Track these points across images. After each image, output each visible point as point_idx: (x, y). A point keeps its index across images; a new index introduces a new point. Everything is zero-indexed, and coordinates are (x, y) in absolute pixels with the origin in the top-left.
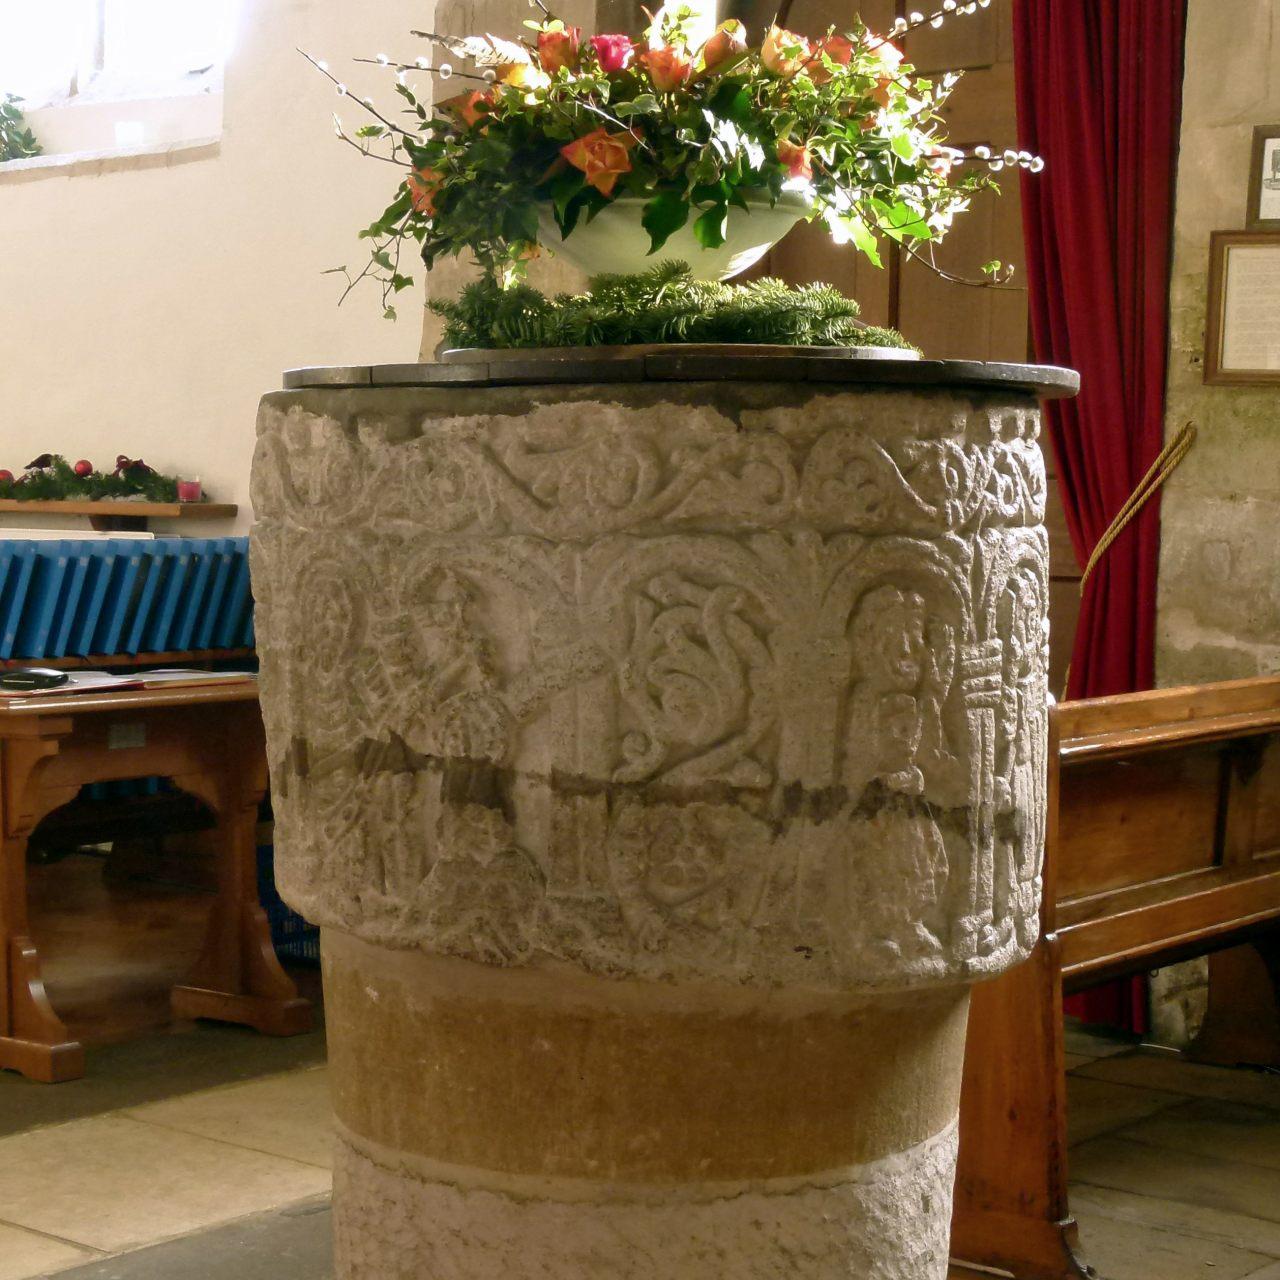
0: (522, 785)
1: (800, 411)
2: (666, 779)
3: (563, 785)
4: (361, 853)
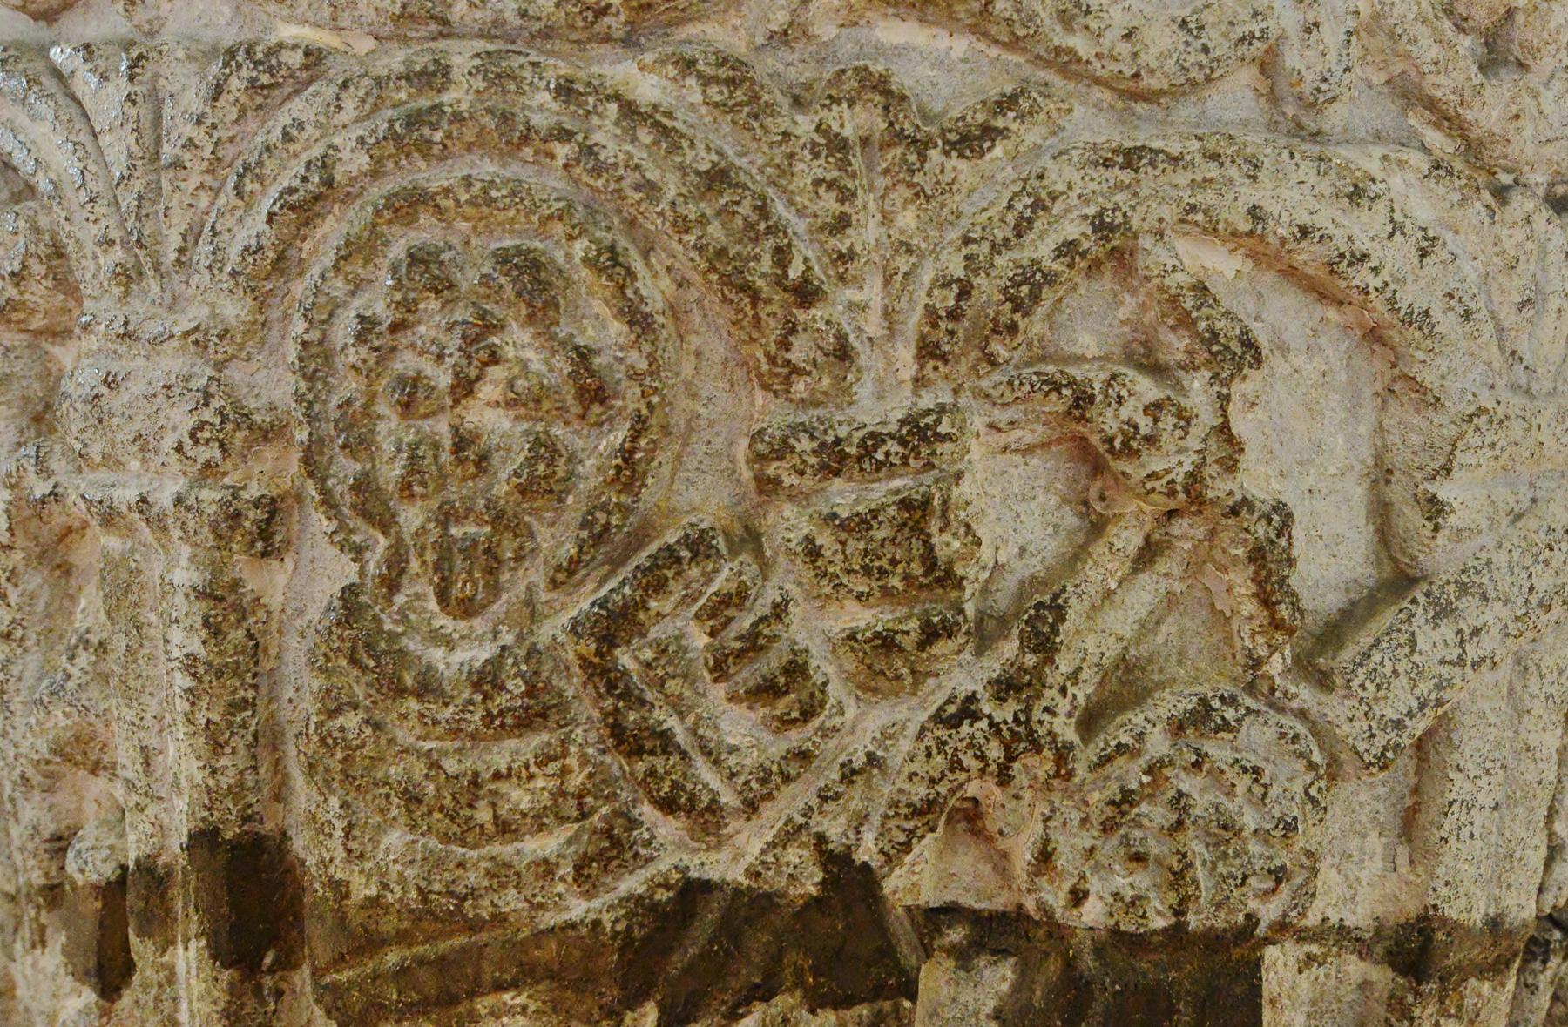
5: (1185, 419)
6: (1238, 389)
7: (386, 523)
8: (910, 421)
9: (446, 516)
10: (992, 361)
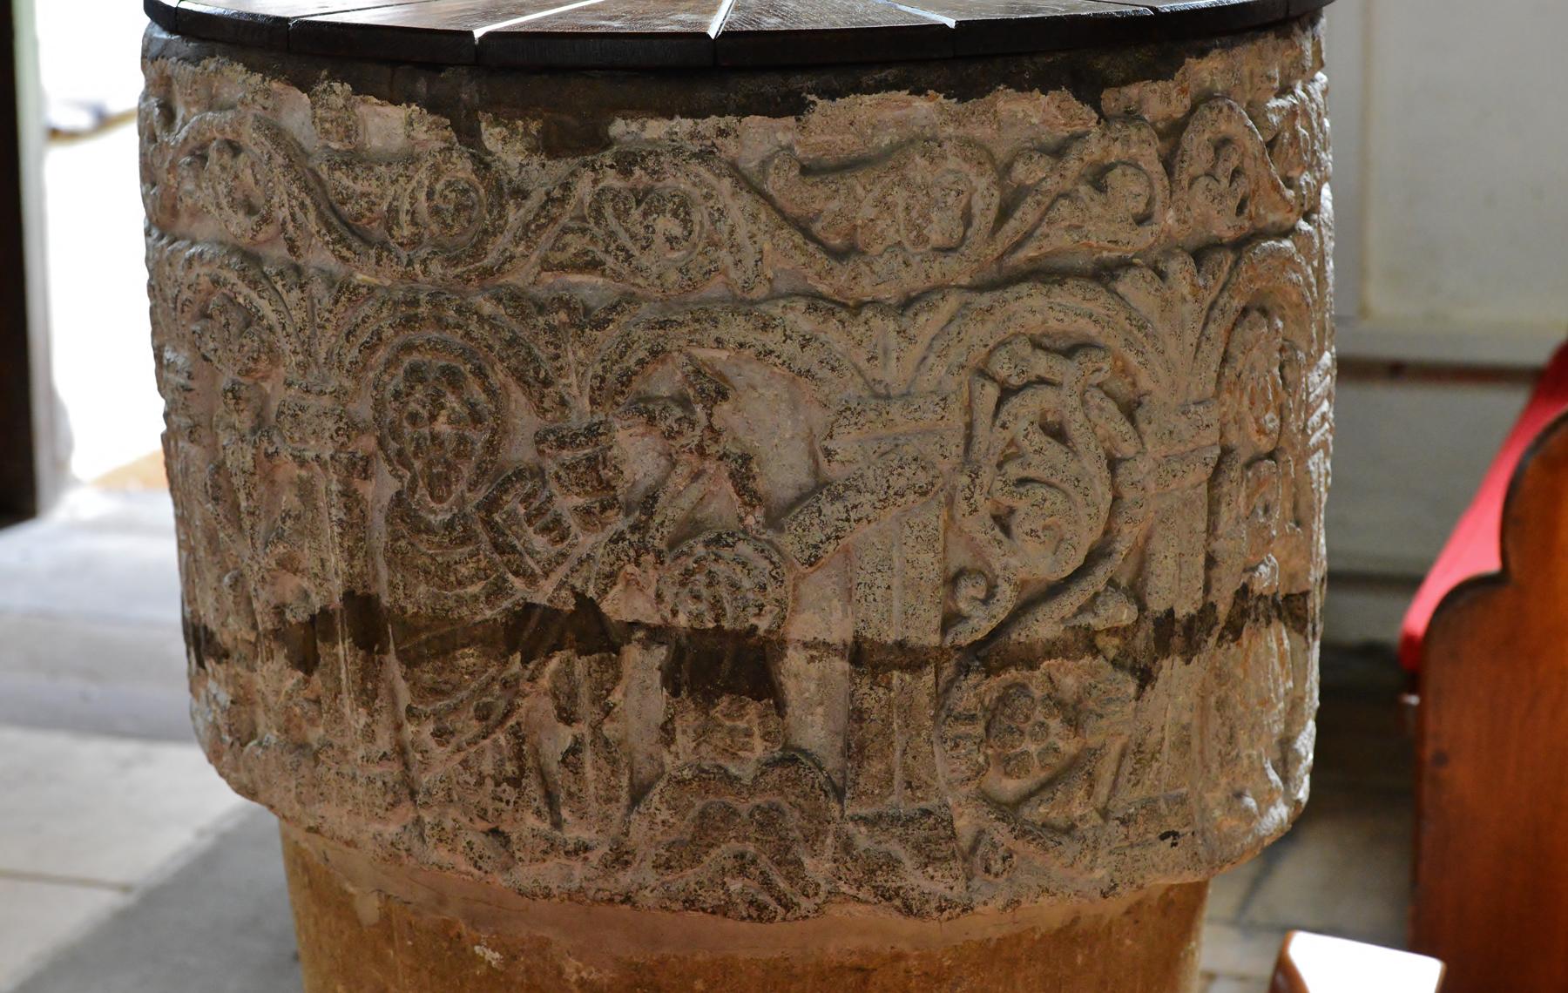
0: (795, 659)
1: (1171, 84)
2: (1017, 635)
3: (862, 656)
4: (510, 768)
5: (693, 425)
6: (716, 410)
7: (409, 467)
8: (588, 429)
9: (430, 464)
10: (618, 405)
